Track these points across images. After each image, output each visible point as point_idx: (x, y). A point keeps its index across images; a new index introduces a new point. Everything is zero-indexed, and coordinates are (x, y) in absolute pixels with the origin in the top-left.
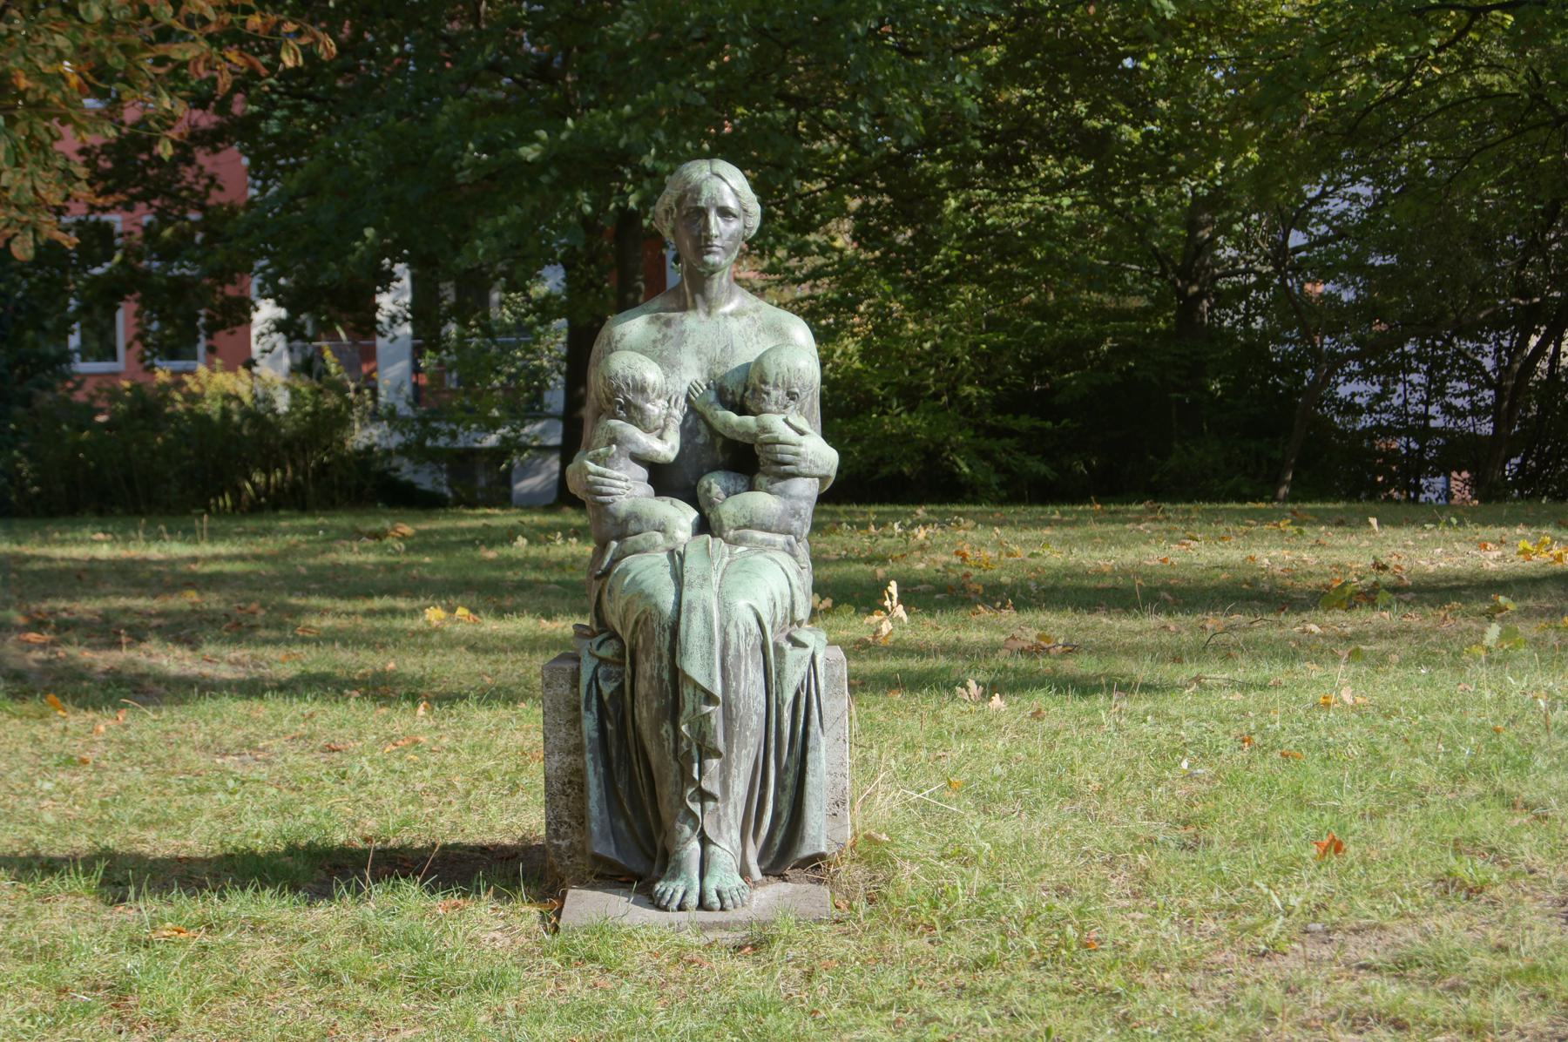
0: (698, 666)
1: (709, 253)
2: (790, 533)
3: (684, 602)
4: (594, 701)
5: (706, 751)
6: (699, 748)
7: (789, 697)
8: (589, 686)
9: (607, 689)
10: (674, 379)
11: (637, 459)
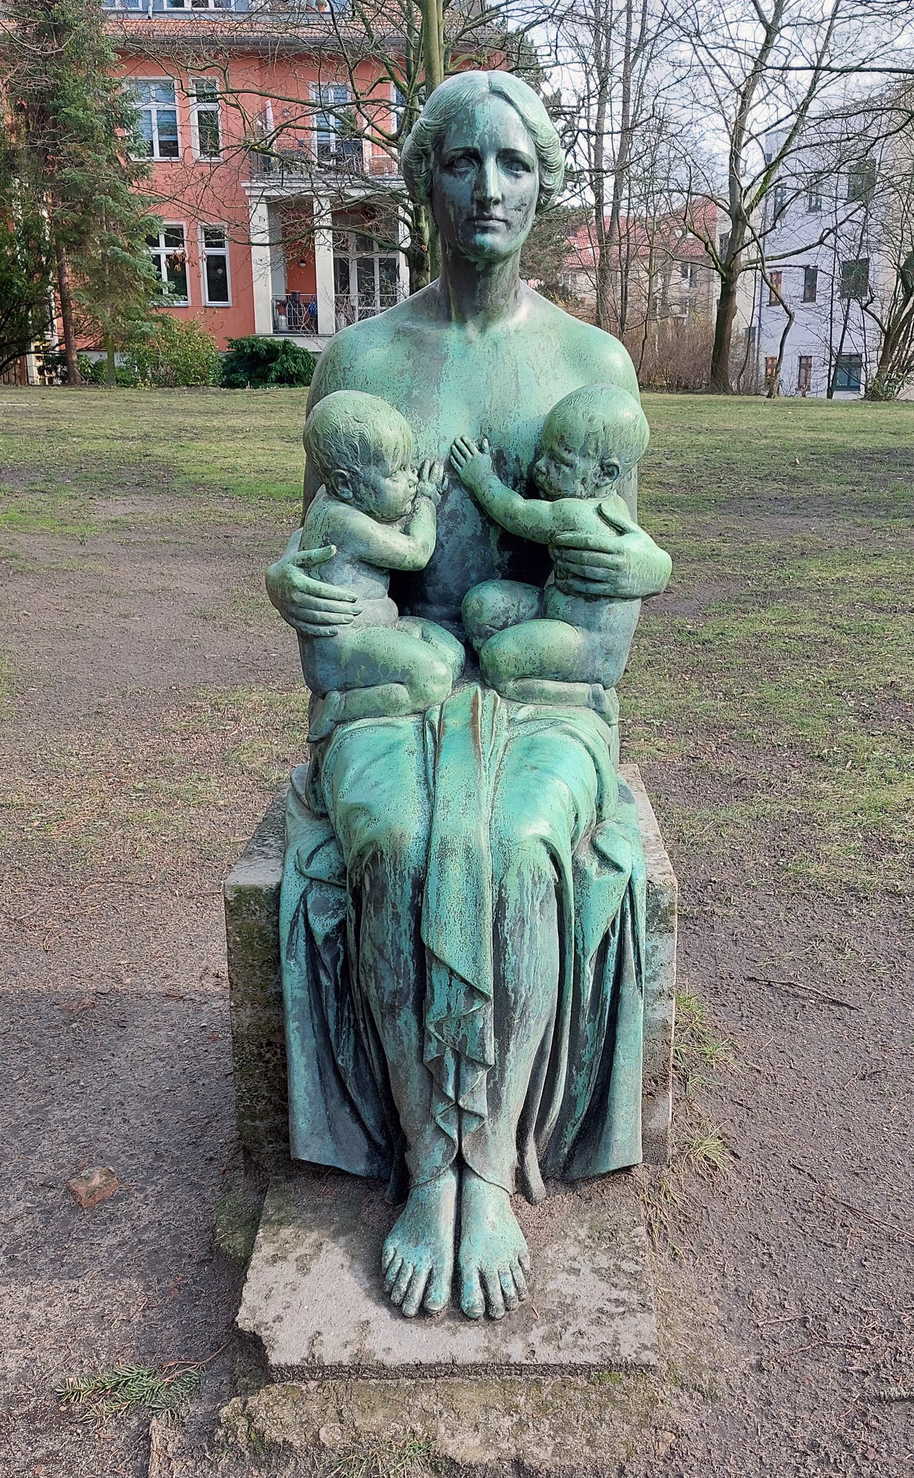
0: (455, 943)
1: (485, 230)
2: (598, 681)
3: (436, 840)
4: (302, 943)
5: (466, 1060)
6: (458, 1055)
7: (593, 945)
8: (294, 924)
9: (322, 926)
10: (429, 435)
11: (371, 564)
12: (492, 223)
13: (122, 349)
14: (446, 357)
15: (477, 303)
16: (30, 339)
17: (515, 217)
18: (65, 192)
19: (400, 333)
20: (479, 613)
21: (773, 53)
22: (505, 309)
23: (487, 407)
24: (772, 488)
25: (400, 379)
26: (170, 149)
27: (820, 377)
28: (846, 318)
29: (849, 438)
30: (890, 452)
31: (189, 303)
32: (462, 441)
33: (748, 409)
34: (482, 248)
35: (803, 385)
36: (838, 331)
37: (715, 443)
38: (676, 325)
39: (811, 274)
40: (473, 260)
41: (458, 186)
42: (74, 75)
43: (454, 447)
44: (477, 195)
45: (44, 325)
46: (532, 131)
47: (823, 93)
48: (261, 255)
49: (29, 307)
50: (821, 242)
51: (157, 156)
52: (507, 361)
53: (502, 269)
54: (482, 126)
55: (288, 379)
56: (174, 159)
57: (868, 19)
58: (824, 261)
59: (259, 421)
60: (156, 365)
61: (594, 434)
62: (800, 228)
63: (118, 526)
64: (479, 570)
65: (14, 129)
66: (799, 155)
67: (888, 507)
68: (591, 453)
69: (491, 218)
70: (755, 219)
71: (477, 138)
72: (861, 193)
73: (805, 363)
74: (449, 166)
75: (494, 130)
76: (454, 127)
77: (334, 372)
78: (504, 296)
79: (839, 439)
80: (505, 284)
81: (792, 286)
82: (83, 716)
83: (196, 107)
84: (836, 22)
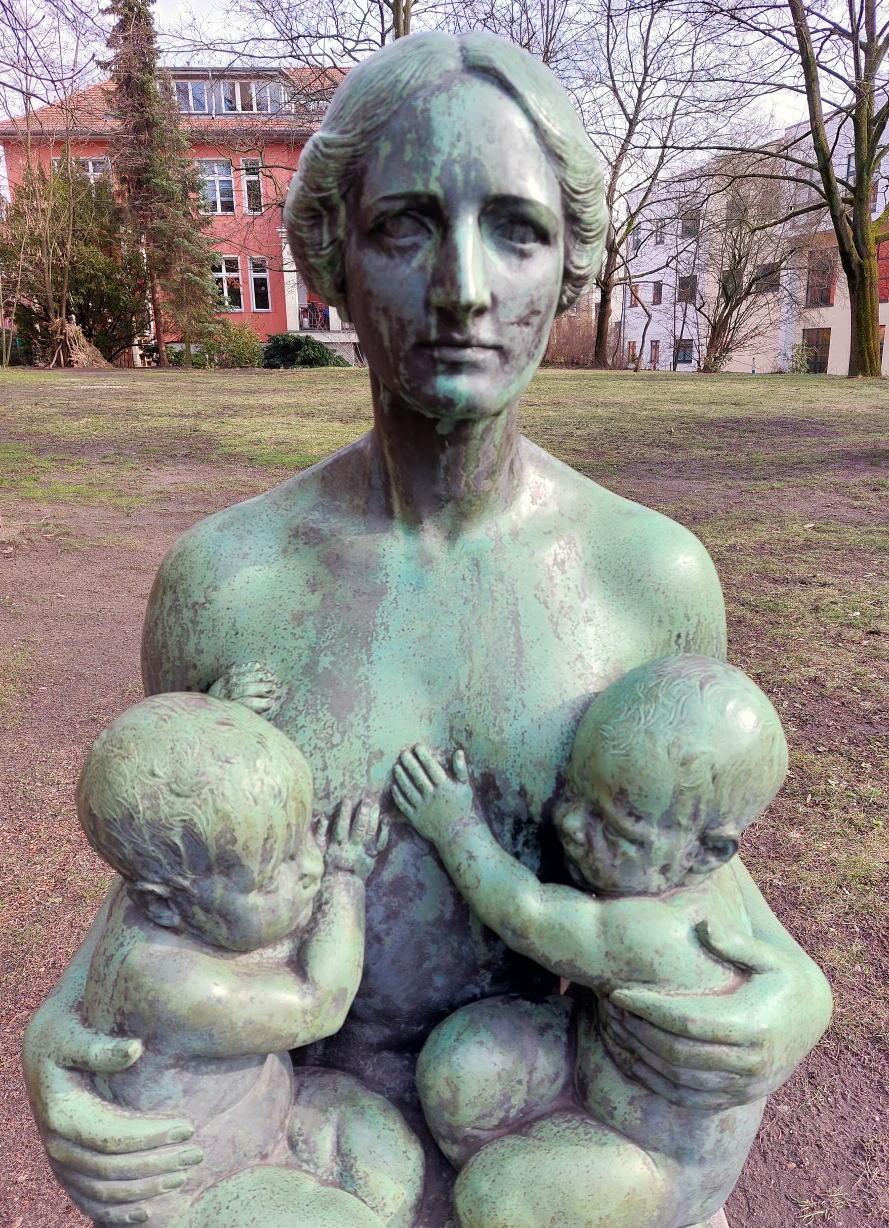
1: (455, 368)
10: (350, 751)
12: (470, 354)
13: (196, 342)
14: (381, 591)
15: (441, 489)
16: (133, 336)
17: (518, 338)
18: (155, 236)
19: (303, 537)
20: (453, 1105)
21: (635, 137)
22: (493, 496)
23: (462, 687)
24: (657, 453)
25: (298, 631)
26: (228, 206)
27: (666, 355)
28: (685, 316)
29: (705, 410)
30: (737, 421)
31: (243, 310)
32: (416, 755)
33: (627, 384)
34: (449, 403)
35: (654, 360)
36: (679, 325)
37: (610, 415)
38: (569, 320)
39: (658, 287)
40: (430, 415)
41: (399, 276)
42: (160, 157)
43: (399, 769)
44: (438, 296)
45: (144, 326)
46: (554, 155)
47: (668, 165)
48: (291, 278)
49: (133, 314)
50: (667, 265)
51: (219, 211)
52: (497, 595)
53: (488, 429)
54: (447, 144)
55: (309, 362)
56: (229, 213)
57: (698, 115)
58: (669, 279)
59: (281, 399)
60: (220, 353)
61: (692, 789)
62: (652, 257)
63: (164, 497)
64: (449, 972)
65: (120, 194)
66: (651, 207)
67: (748, 470)
68: (684, 822)
69: (466, 344)
70: (622, 250)
71: (436, 172)
72: (691, 231)
73: (655, 345)
74: (376, 233)
75: (475, 154)
76: (385, 148)
77: (176, 609)
78: (492, 473)
79: (698, 410)
80: (493, 454)
81: (646, 294)
82: (80, 723)
83: (246, 178)
84: (676, 117)
